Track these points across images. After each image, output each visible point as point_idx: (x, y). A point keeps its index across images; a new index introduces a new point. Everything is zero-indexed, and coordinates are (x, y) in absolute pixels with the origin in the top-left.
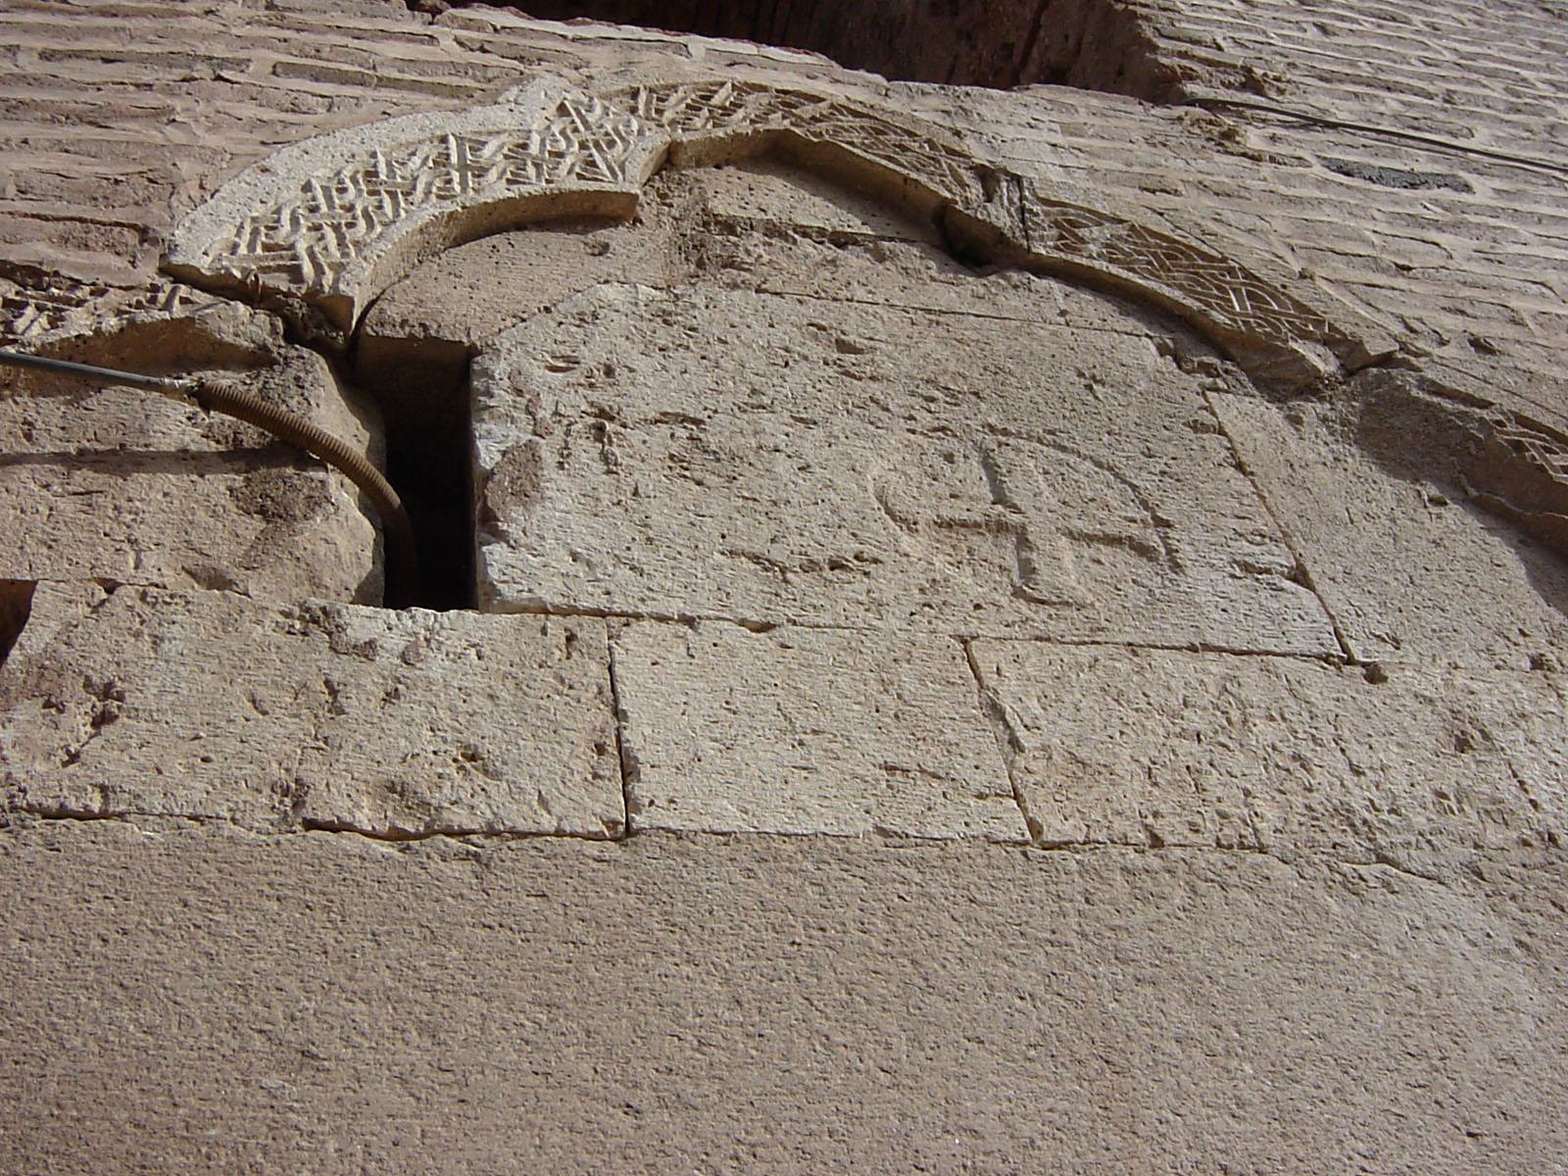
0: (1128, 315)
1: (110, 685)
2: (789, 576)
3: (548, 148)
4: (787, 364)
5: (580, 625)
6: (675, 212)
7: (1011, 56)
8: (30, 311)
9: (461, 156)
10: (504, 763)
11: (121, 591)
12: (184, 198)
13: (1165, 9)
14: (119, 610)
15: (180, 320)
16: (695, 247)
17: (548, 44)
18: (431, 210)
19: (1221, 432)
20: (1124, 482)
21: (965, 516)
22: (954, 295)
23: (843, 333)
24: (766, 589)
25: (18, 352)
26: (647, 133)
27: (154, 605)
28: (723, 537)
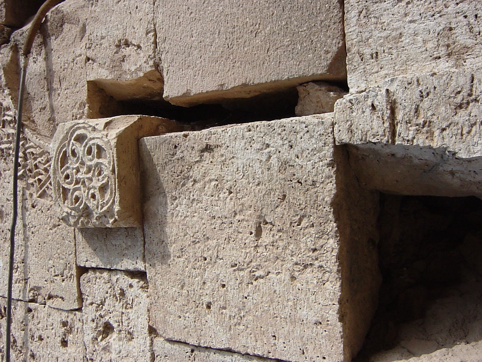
15: (4, 71)
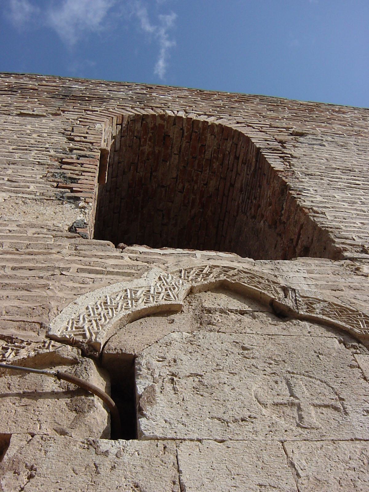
0: (329, 331)
1: (33, 466)
2: (229, 424)
3: (156, 291)
4: (227, 355)
5: (168, 443)
6: (193, 308)
7: (293, 242)
8: (10, 351)
9: (131, 296)
10: (146, 488)
11: (35, 437)
12: (53, 313)
13: (337, 228)
14: (35, 442)
15: (52, 352)
16: (199, 318)
17: (155, 257)
18: (123, 313)
19: (359, 367)
20: (329, 386)
21: (282, 401)
22: (276, 329)
23: (244, 344)
24: (222, 429)
25: (6, 364)
26: (185, 284)
27: (45, 441)
28: (209, 413)
